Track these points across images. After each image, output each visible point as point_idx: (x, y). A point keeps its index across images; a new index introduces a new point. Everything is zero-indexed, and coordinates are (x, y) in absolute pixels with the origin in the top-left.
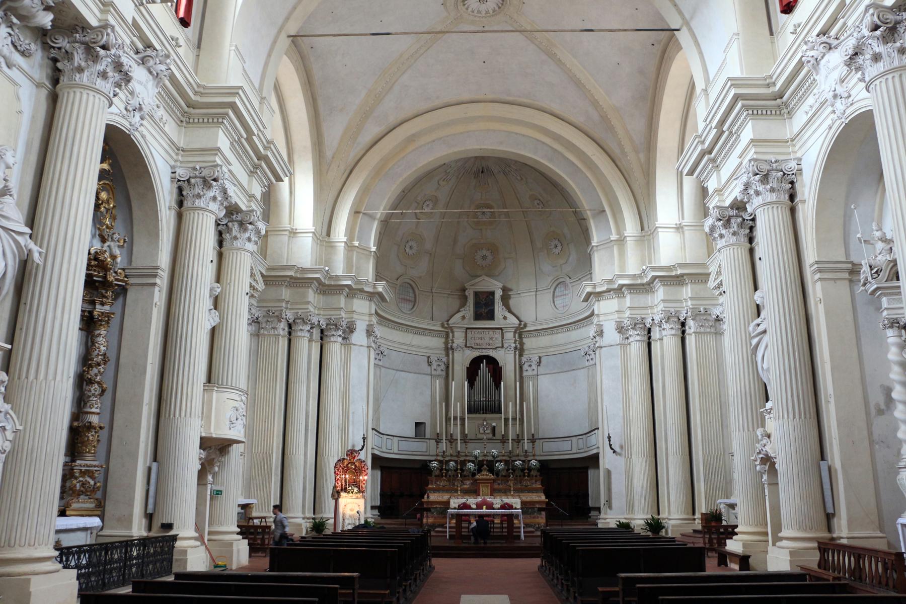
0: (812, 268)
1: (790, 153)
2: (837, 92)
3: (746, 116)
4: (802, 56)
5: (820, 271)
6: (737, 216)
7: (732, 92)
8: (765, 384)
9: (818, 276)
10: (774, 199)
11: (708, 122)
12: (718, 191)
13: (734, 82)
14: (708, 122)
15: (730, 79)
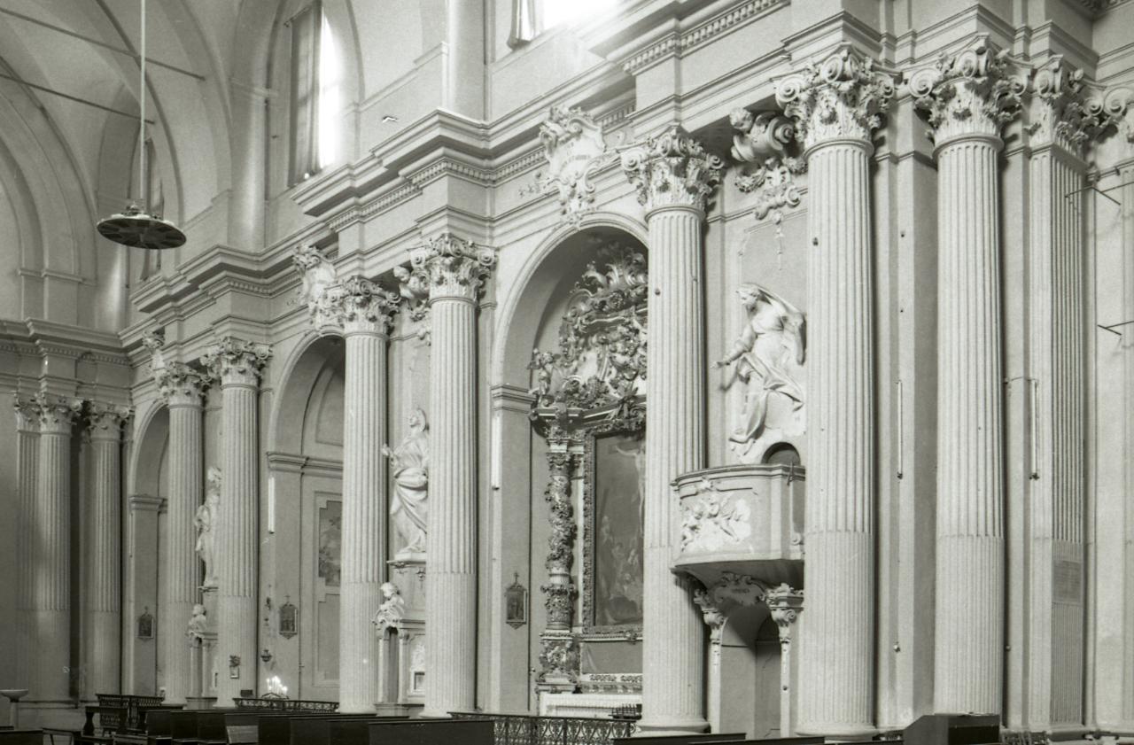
0: (495, 391)
1: (484, 237)
2: (577, 188)
3: (671, 48)
4: (542, 124)
5: (504, 396)
6: (195, 376)
7: (437, 132)
8: (203, 563)
9: (499, 403)
10: (244, 382)
11: (183, 272)
12: (361, 254)
13: (444, 120)
14: (183, 272)
15: (439, 113)
